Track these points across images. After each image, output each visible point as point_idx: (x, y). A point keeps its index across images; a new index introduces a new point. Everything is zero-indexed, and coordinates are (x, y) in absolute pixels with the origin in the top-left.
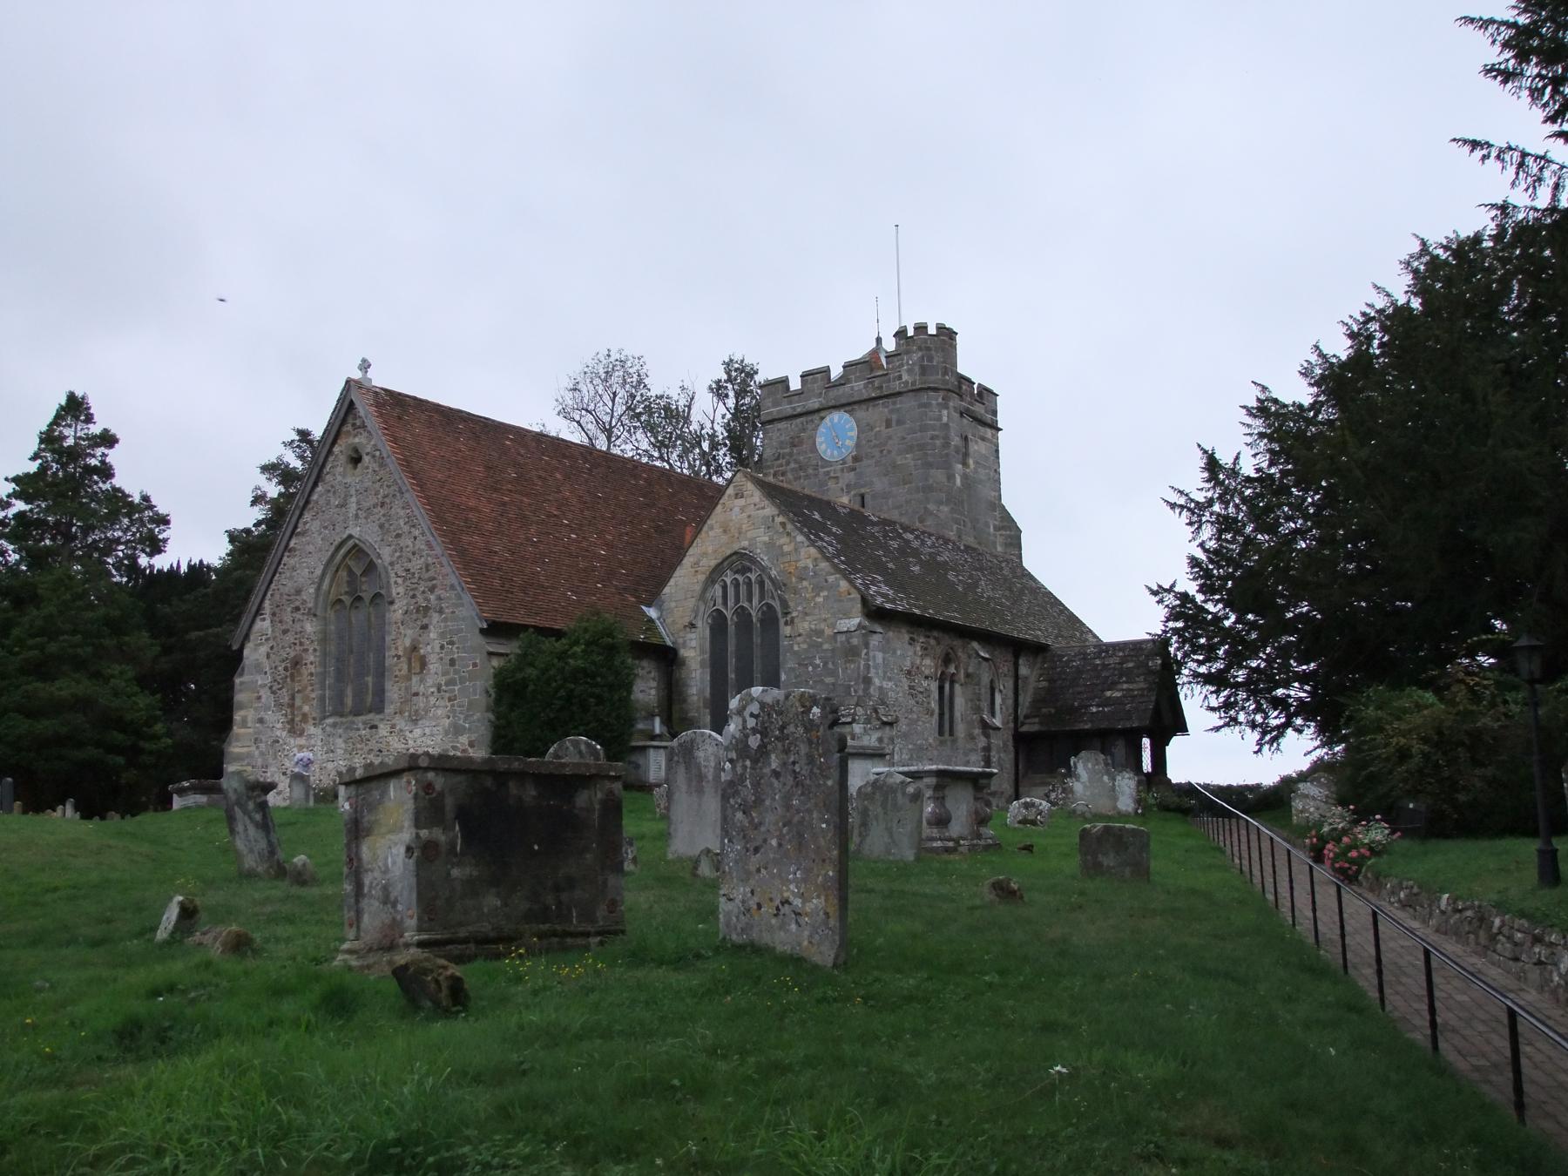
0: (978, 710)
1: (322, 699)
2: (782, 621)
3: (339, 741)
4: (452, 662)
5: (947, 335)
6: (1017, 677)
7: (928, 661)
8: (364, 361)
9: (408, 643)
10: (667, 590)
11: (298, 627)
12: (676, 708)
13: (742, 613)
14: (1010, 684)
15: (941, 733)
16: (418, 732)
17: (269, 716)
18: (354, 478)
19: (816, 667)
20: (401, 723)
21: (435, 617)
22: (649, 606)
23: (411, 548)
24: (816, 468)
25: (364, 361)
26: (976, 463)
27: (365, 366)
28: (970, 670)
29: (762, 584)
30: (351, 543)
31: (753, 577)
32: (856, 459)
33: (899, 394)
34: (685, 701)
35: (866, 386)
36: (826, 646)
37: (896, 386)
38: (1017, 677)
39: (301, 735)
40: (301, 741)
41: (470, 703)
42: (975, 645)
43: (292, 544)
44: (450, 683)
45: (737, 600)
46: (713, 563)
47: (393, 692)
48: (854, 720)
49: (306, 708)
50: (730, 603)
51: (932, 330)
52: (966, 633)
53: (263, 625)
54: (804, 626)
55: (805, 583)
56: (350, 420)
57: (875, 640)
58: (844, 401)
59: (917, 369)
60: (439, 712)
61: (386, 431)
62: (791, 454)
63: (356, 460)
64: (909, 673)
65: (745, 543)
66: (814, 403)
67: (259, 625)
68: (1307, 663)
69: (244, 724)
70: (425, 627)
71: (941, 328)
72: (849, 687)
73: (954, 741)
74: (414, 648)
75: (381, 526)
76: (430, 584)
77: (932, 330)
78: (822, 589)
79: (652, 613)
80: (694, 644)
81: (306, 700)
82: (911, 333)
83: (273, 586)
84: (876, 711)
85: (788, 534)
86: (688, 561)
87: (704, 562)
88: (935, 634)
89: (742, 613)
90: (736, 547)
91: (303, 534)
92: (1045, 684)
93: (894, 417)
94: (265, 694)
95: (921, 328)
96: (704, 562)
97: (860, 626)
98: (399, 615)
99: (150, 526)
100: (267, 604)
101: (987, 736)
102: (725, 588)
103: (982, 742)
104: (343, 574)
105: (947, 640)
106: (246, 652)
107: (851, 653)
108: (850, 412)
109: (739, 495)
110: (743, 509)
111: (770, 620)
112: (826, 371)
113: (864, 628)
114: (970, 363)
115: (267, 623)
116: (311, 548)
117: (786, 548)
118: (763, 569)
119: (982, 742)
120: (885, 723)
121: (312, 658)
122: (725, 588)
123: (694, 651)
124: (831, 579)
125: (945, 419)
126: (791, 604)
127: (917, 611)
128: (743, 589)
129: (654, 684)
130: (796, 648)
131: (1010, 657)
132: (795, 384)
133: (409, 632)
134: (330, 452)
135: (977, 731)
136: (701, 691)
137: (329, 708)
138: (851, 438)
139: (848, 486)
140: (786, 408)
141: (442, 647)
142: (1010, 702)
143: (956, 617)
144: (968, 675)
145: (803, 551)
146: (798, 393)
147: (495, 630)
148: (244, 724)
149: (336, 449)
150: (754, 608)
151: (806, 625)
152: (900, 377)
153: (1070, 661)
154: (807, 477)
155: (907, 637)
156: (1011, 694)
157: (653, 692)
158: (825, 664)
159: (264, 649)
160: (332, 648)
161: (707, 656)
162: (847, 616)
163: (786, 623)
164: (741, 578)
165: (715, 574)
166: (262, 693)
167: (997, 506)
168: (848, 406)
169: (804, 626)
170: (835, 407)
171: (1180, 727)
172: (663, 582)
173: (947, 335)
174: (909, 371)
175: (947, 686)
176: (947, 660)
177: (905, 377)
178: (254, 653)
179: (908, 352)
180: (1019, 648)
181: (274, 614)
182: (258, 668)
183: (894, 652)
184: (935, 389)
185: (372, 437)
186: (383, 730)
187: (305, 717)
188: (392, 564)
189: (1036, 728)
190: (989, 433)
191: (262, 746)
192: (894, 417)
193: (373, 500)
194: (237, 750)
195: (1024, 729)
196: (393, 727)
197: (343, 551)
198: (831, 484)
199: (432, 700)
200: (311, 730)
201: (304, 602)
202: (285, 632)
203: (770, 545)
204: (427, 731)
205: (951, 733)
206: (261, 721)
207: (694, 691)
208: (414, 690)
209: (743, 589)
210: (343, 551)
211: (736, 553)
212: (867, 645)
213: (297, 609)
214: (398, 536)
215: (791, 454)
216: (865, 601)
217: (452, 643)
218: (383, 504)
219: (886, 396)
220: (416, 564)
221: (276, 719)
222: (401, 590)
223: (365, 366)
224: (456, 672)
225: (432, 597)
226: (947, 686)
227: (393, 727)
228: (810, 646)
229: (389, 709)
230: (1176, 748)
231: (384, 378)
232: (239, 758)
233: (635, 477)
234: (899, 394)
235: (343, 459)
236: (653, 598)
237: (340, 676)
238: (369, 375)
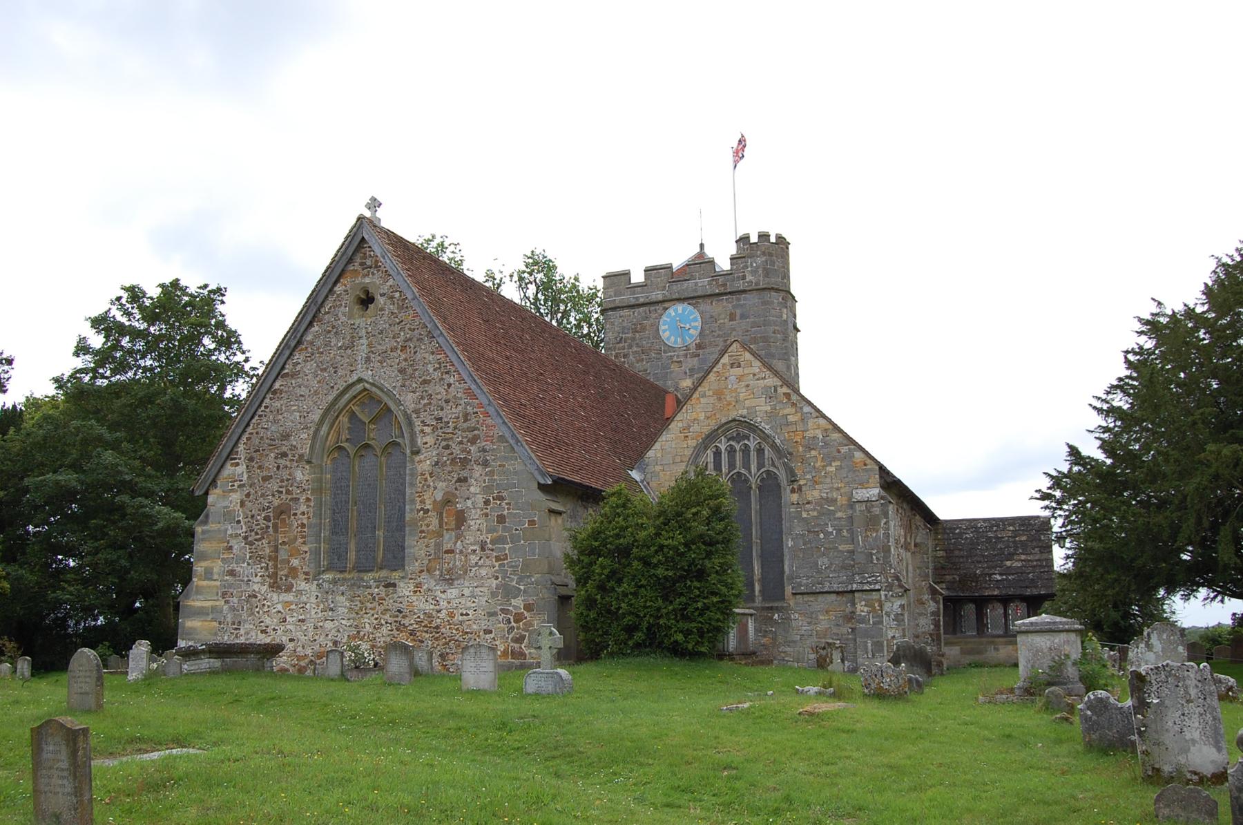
1: (317, 552)
4: (501, 519)
9: (439, 496)
10: (651, 453)
11: (285, 474)
16: (452, 592)
17: (242, 568)
18: (363, 322)
19: (827, 534)
20: (428, 582)
21: (478, 470)
23: (443, 395)
24: (659, 352)
25: (374, 199)
27: (374, 204)
29: (760, 451)
30: (359, 387)
31: (752, 444)
32: (699, 346)
33: (744, 291)
35: (710, 283)
36: (839, 515)
39: (289, 589)
40: (289, 597)
41: (526, 565)
43: (277, 385)
45: (732, 465)
46: (706, 430)
47: (417, 548)
49: (295, 562)
50: (753, 468)
53: (237, 470)
54: (814, 494)
55: (813, 453)
56: (358, 260)
58: (687, 295)
60: (483, 572)
61: (375, 271)
62: (633, 339)
63: (366, 300)
65: (745, 412)
66: (658, 295)
67: (229, 470)
69: (208, 575)
74: (448, 501)
75: (402, 371)
76: (470, 435)
78: (834, 459)
79: (635, 475)
81: (296, 553)
83: (250, 429)
85: (794, 404)
86: (675, 426)
87: (696, 428)
90: (733, 415)
91: (293, 375)
92: (941, 553)
93: (738, 312)
94: (237, 545)
96: (696, 428)
100: (241, 447)
102: (717, 454)
104: (344, 419)
106: (210, 499)
108: (695, 306)
110: (740, 379)
111: (770, 486)
115: (242, 469)
116: (303, 391)
117: (791, 418)
118: (765, 437)
121: (303, 508)
122: (717, 454)
125: (785, 317)
126: (799, 473)
128: (738, 456)
130: (804, 515)
133: (441, 485)
134: (331, 291)
137: (324, 563)
139: (691, 370)
140: (629, 298)
141: (487, 502)
145: (810, 423)
147: (557, 488)
148: (208, 575)
149: (339, 289)
151: (816, 493)
152: (744, 277)
153: (961, 534)
154: (649, 360)
158: (839, 531)
159: (236, 497)
160: (327, 498)
162: (863, 485)
163: (793, 491)
166: (233, 543)
170: (678, 300)
174: (754, 272)
177: (749, 278)
179: (751, 256)
181: (251, 459)
182: (228, 516)
185: (391, 280)
186: (405, 589)
187: (293, 571)
188: (417, 411)
192: (738, 312)
193: (389, 343)
194: (198, 604)
196: (418, 585)
197: (347, 396)
199: (474, 559)
203: (771, 416)
204: (467, 592)
206: (232, 573)
208: (447, 547)
209: (738, 456)
210: (347, 396)
211: (734, 420)
213: (284, 455)
214: (425, 382)
215: (633, 339)
217: (501, 498)
218: (404, 348)
219: (730, 293)
220: (450, 413)
222: (430, 440)
224: (504, 529)
227: (418, 585)
228: (821, 514)
229: (412, 567)
232: (201, 612)
234: (744, 291)
235: (348, 299)
236: (636, 457)
237: (338, 528)
238: (378, 215)
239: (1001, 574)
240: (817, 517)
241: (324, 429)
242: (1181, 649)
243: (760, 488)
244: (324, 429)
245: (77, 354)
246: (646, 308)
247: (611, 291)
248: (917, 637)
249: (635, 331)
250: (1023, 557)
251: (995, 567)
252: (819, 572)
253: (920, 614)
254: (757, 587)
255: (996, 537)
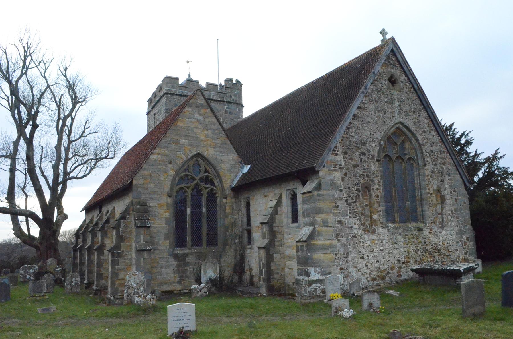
3: (400, 237)
5: (170, 80)
9: (435, 187)
16: (444, 233)
20: (435, 229)
44: (456, 210)
47: (429, 212)
94: (342, 204)
98: (428, 172)
112: (177, 79)
121: (377, 186)
141: (451, 192)
152: (231, 97)
177: (233, 97)
186: (426, 232)
191: (344, 240)
196: (431, 230)
200: (380, 230)
201: (369, 151)
202: (355, 166)
204: (448, 233)
206: (340, 222)
213: (364, 154)
225: (444, 167)
227: (431, 230)
229: (428, 221)
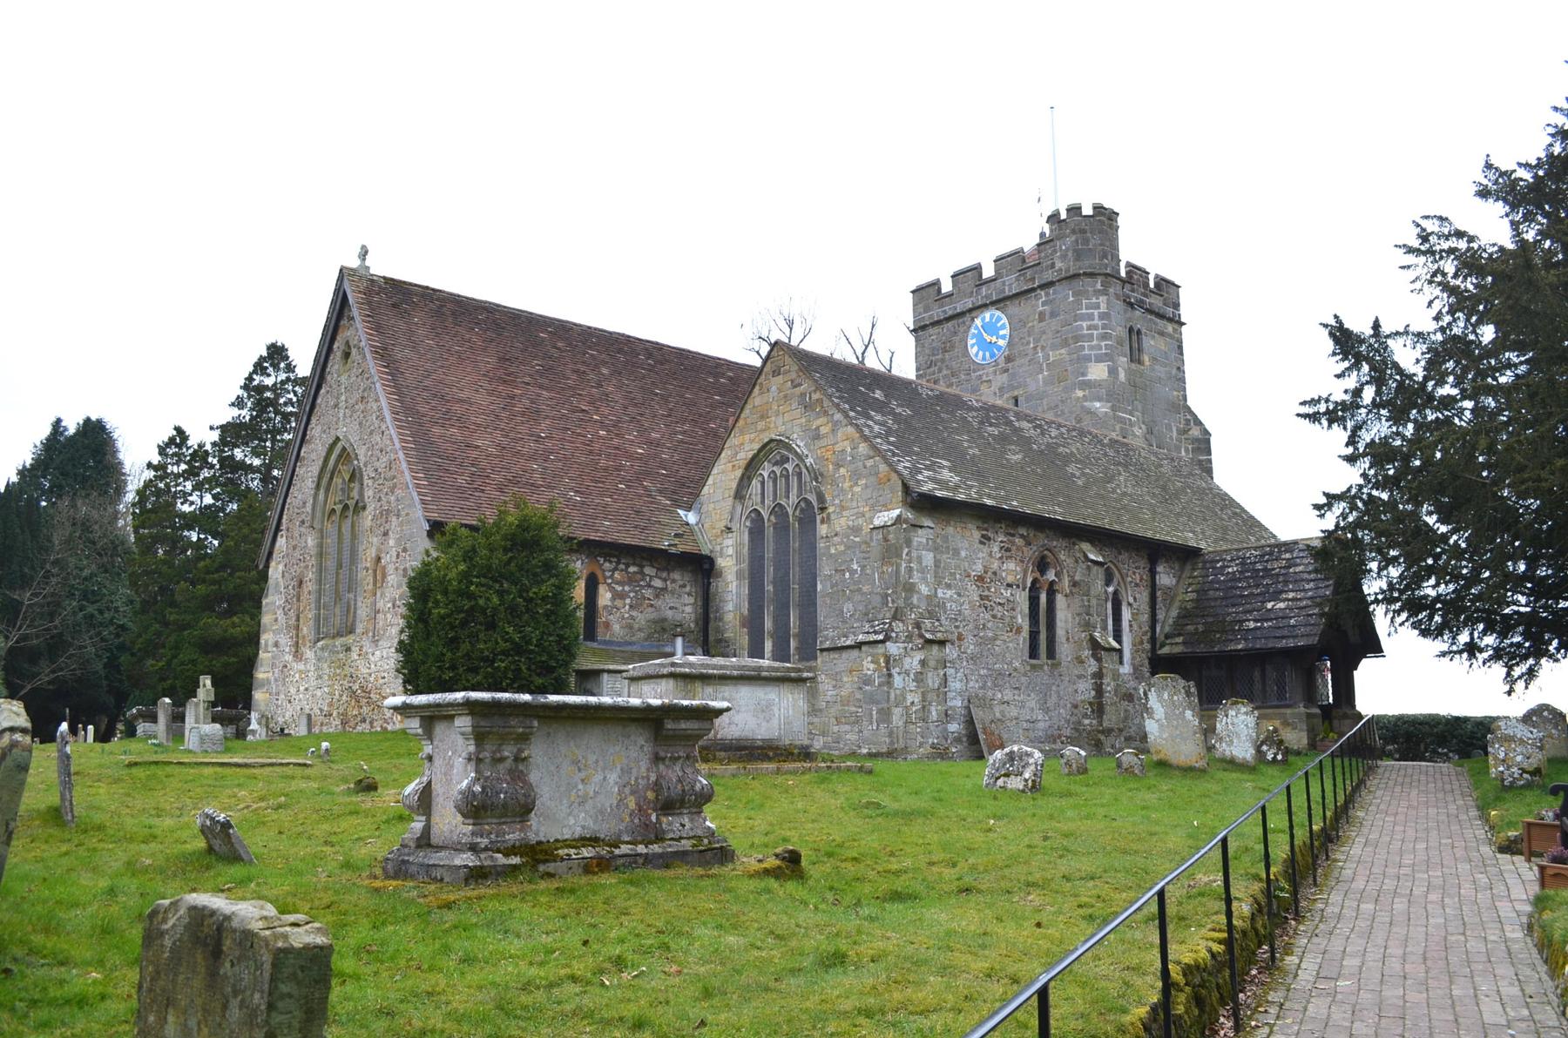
0: (1088, 626)
2: (819, 518)
6: (1153, 587)
7: (1011, 565)
8: (364, 247)
10: (705, 490)
12: (712, 625)
13: (778, 511)
14: (1144, 596)
15: (1033, 653)
22: (689, 509)
25: (364, 247)
26: (1154, 359)
27: (364, 253)
28: (1077, 578)
32: (1009, 359)
34: (721, 619)
35: (1017, 279)
37: (1049, 276)
38: (1153, 587)
42: (1086, 546)
48: (887, 638)
51: (1087, 211)
52: (1073, 532)
55: (842, 471)
57: (920, 537)
59: (1070, 254)
62: (943, 361)
64: (980, 579)
68: (1441, 521)
70: (386, 534)
71: (1098, 208)
72: (887, 595)
73: (1056, 666)
77: (1087, 211)
79: (691, 518)
80: (730, 551)
82: (1063, 216)
84: (918, 625)
88: (1023, 531)
89: (778, 511)
95: (1075, 210)
97: (899, 519)
99: (66, 429)
101: (1099, 660)
102: (763, 483)
103: (1092, 666)
105: (1042, 539)
107: (890, 553)
109: (776, 373)
111: (810, 515)
113: (906, 521)
114: (1137, 247)
119: (1092, 666)
120: (929, 642)
123: (730, 559)
124: (870, 463)
126: (828, 498)
127: (989, 502)
129: (692, 600)
131: (1143, 563)
132: (947, 287)
135: (1087, 653)
136: (738, 607)
138: (1003, 337)
139: (1001, 389)
142: (1145, 617)
143: (1057, 513)
144: (1075, 584)
146: (950, 295)
150: (791, 502)
152: (1053, 266)
153: (1224, 567)
154: (959, 383)
155: (977, 535)
156: (1145, 607)
157: (688, 609)
158: (863, 568)
161: (745, 566)
163: (823, 522)
164: (777, 470)
165: (752, 466)
167: (1181, 406)
168: (999, 303)
169: (841, 523)
170: (985, 306)
171: (1373, 647)
172: (702, 482)
173: (1105, 218)
174: (1064, 257)
175: (1043, 597)
176: (1042, 566)
177: (1059, 265)
178: (276, 571)
180: (1155, 552)
183: (956, 552)
184: (1092, 275)
189: (1178, 649)
190: (1170, 328)
195: (1166, 650)
198: (983, 388)
205: (1051, 653)
207: (730, 607)
209: (781, 483)
212: (908, 543)
215: (943, 361)
216: (906, 488)
217: (405, 550)
221: (285, 641)
223: (364, 253)
226: (1043, 597)
228: (848, 548)
230: (1367, 674)
231: (382, 266)
233: (716, 376)
239: (1256, 621)
240: (843, 552)
241: (321, 496)
242: (1189, 714)
243: (800, 521)
244: (321, 496)
245: (1347, 445)
246: (954, 322)
247: (921, 308)
248: (1076, 707)
249: (945, 351)
250: (1291, 595)
251: (1250, 612)
252: (844, 622)
253: (1079, 677)
254: (793, 644)
255: (1265, 569)
